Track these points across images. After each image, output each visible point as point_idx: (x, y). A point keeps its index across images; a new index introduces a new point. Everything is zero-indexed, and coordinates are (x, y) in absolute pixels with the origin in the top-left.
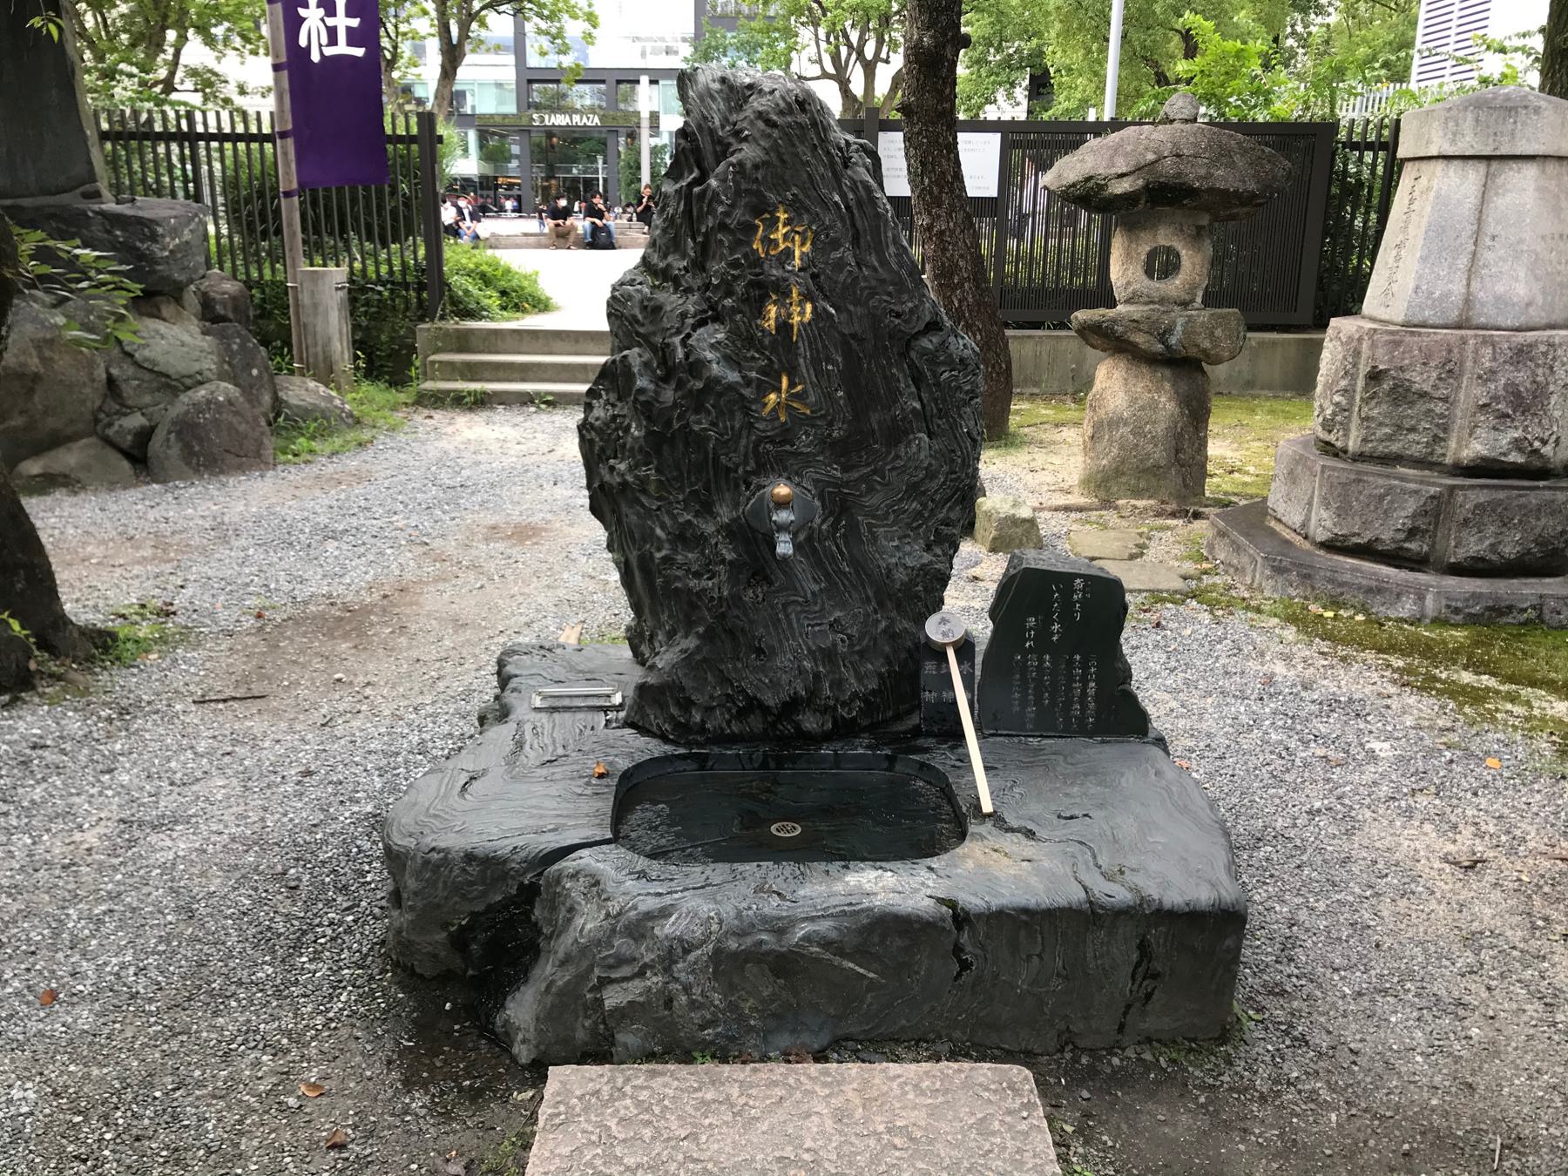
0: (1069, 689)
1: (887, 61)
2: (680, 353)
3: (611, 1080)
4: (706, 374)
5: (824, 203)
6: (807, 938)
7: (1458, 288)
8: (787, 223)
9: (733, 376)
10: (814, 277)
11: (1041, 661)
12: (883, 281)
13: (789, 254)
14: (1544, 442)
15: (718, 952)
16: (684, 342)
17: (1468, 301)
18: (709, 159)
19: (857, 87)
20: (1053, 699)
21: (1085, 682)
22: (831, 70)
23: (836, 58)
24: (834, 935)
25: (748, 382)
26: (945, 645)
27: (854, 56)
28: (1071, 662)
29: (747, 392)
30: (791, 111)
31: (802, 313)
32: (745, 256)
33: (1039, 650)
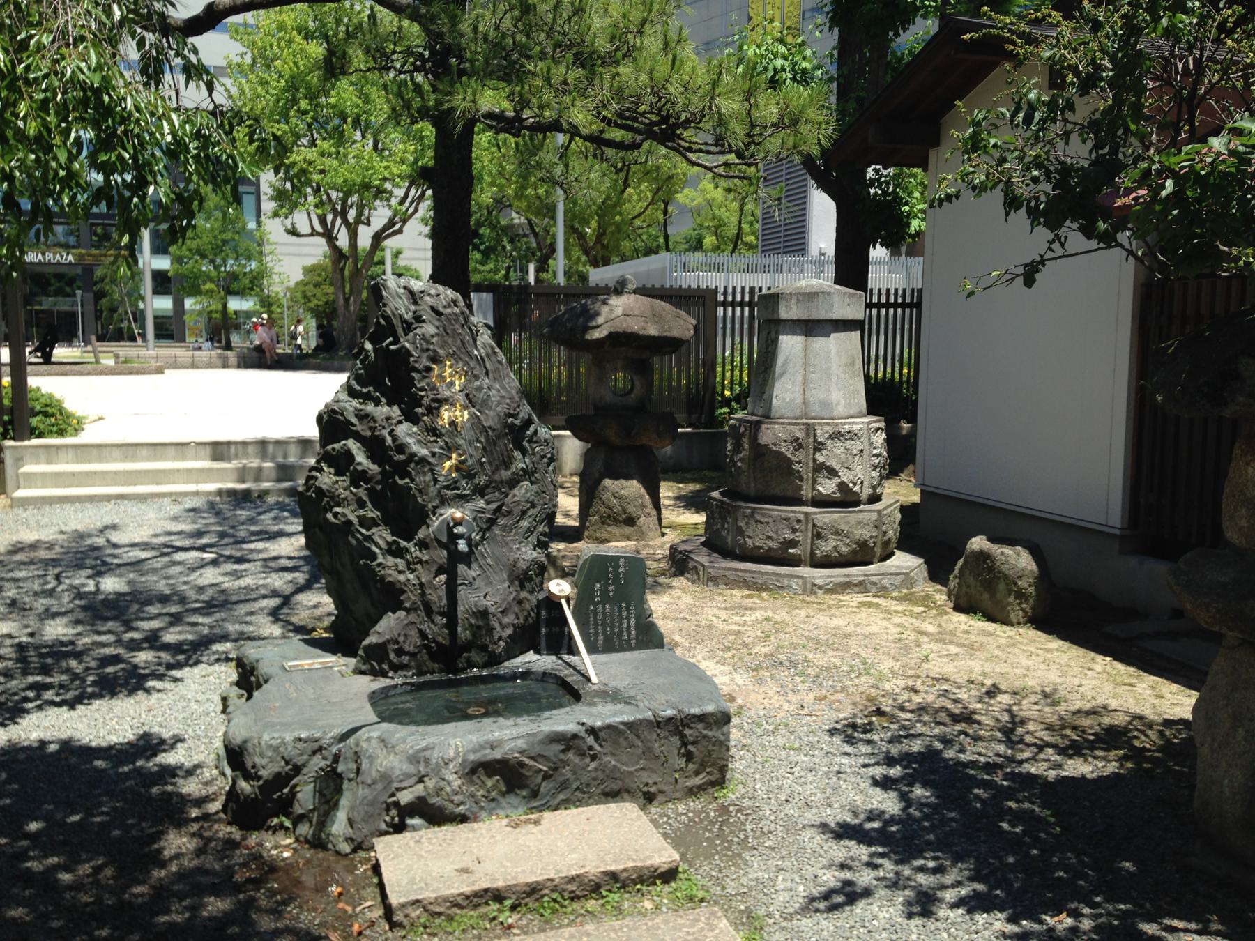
0: (621, 624)
1: (368, 224)
2: (389, 439)
3: (412, 838)
4: (407, 451)
5: (470, 355)
6: (511, 749)
7: (799, 400)
8: (451, 367)
9: (424, 452)
10: (467, 395)
11: (604, 608)
12: (503, 397)
13: (452, 383)
14: (855, 485)
15: (464, 761)
16: (391, 433)
17: (805, 402)
18: (400, 331)
19: (343, 241)
20: (612, 630)
21: (628, 618)
22: (319, 228)
23: (322, 220)
24: (525, 746)
25: (434, 455)
26: (561, 597)
27: (339, 221)
28: (620, 608)
29: (432, 460)
30: (449, 306)
31: (462, 416)
32: (428, 384)
33: (603, 602)
